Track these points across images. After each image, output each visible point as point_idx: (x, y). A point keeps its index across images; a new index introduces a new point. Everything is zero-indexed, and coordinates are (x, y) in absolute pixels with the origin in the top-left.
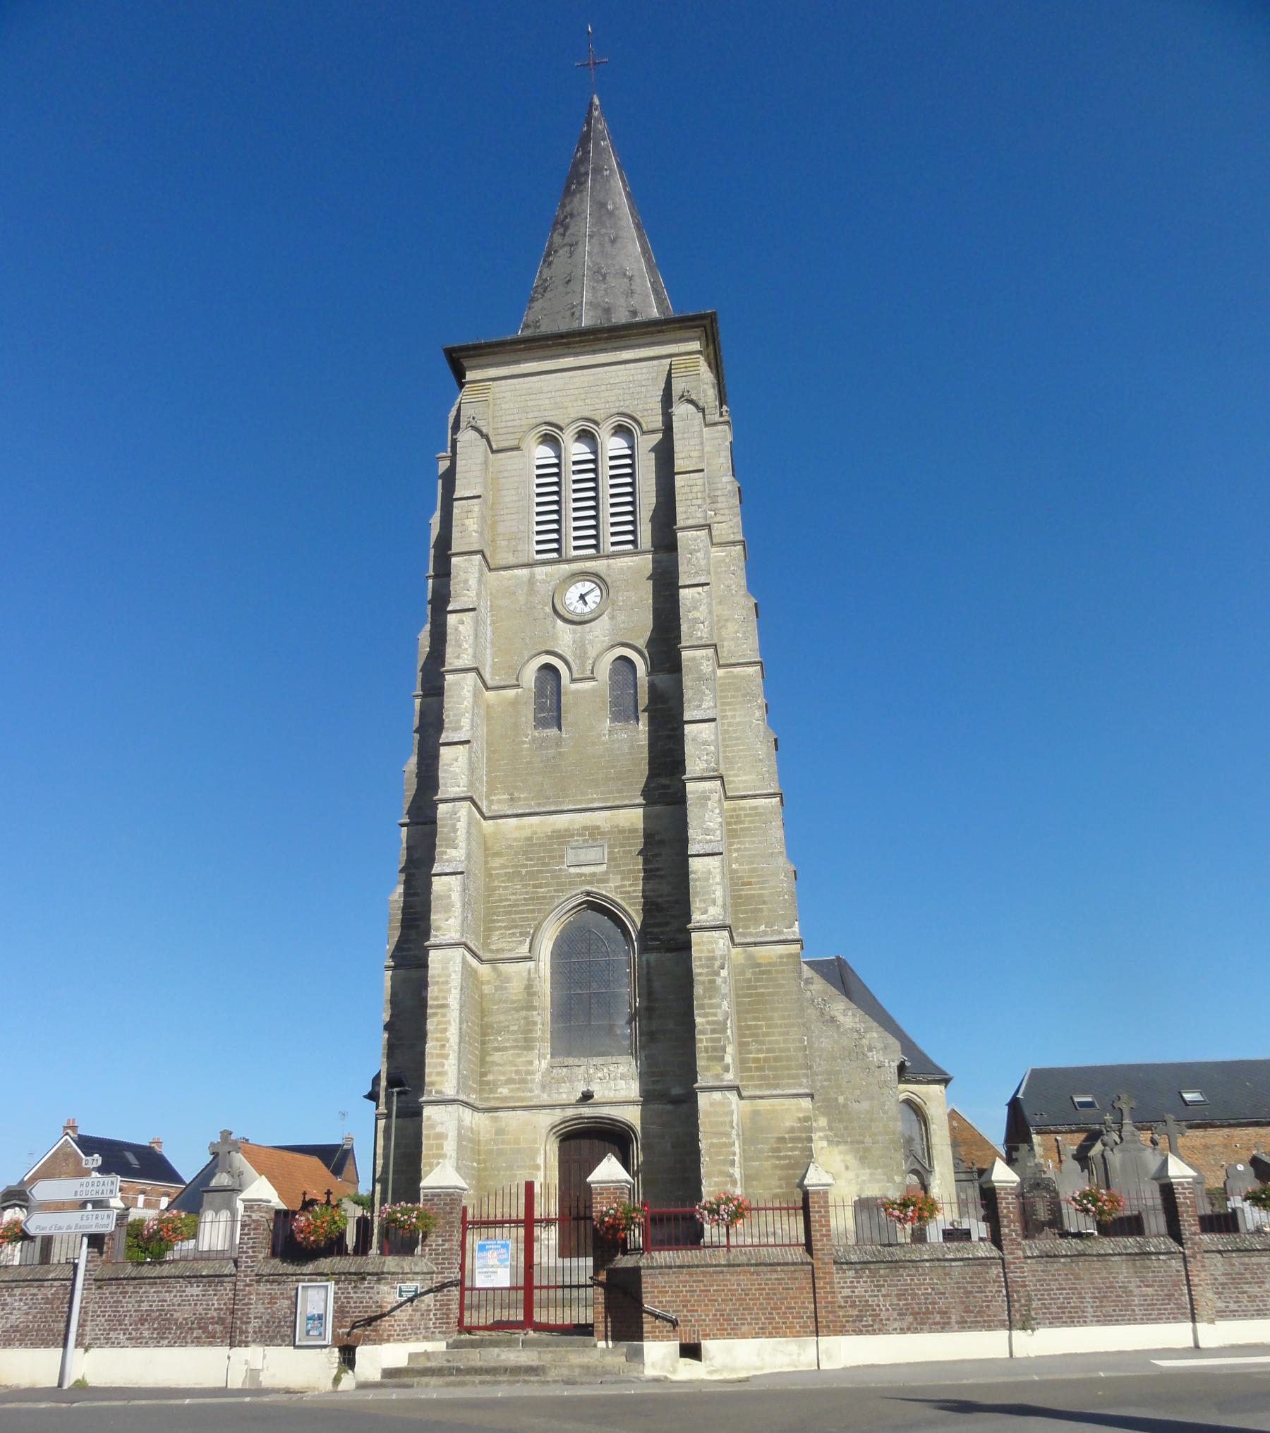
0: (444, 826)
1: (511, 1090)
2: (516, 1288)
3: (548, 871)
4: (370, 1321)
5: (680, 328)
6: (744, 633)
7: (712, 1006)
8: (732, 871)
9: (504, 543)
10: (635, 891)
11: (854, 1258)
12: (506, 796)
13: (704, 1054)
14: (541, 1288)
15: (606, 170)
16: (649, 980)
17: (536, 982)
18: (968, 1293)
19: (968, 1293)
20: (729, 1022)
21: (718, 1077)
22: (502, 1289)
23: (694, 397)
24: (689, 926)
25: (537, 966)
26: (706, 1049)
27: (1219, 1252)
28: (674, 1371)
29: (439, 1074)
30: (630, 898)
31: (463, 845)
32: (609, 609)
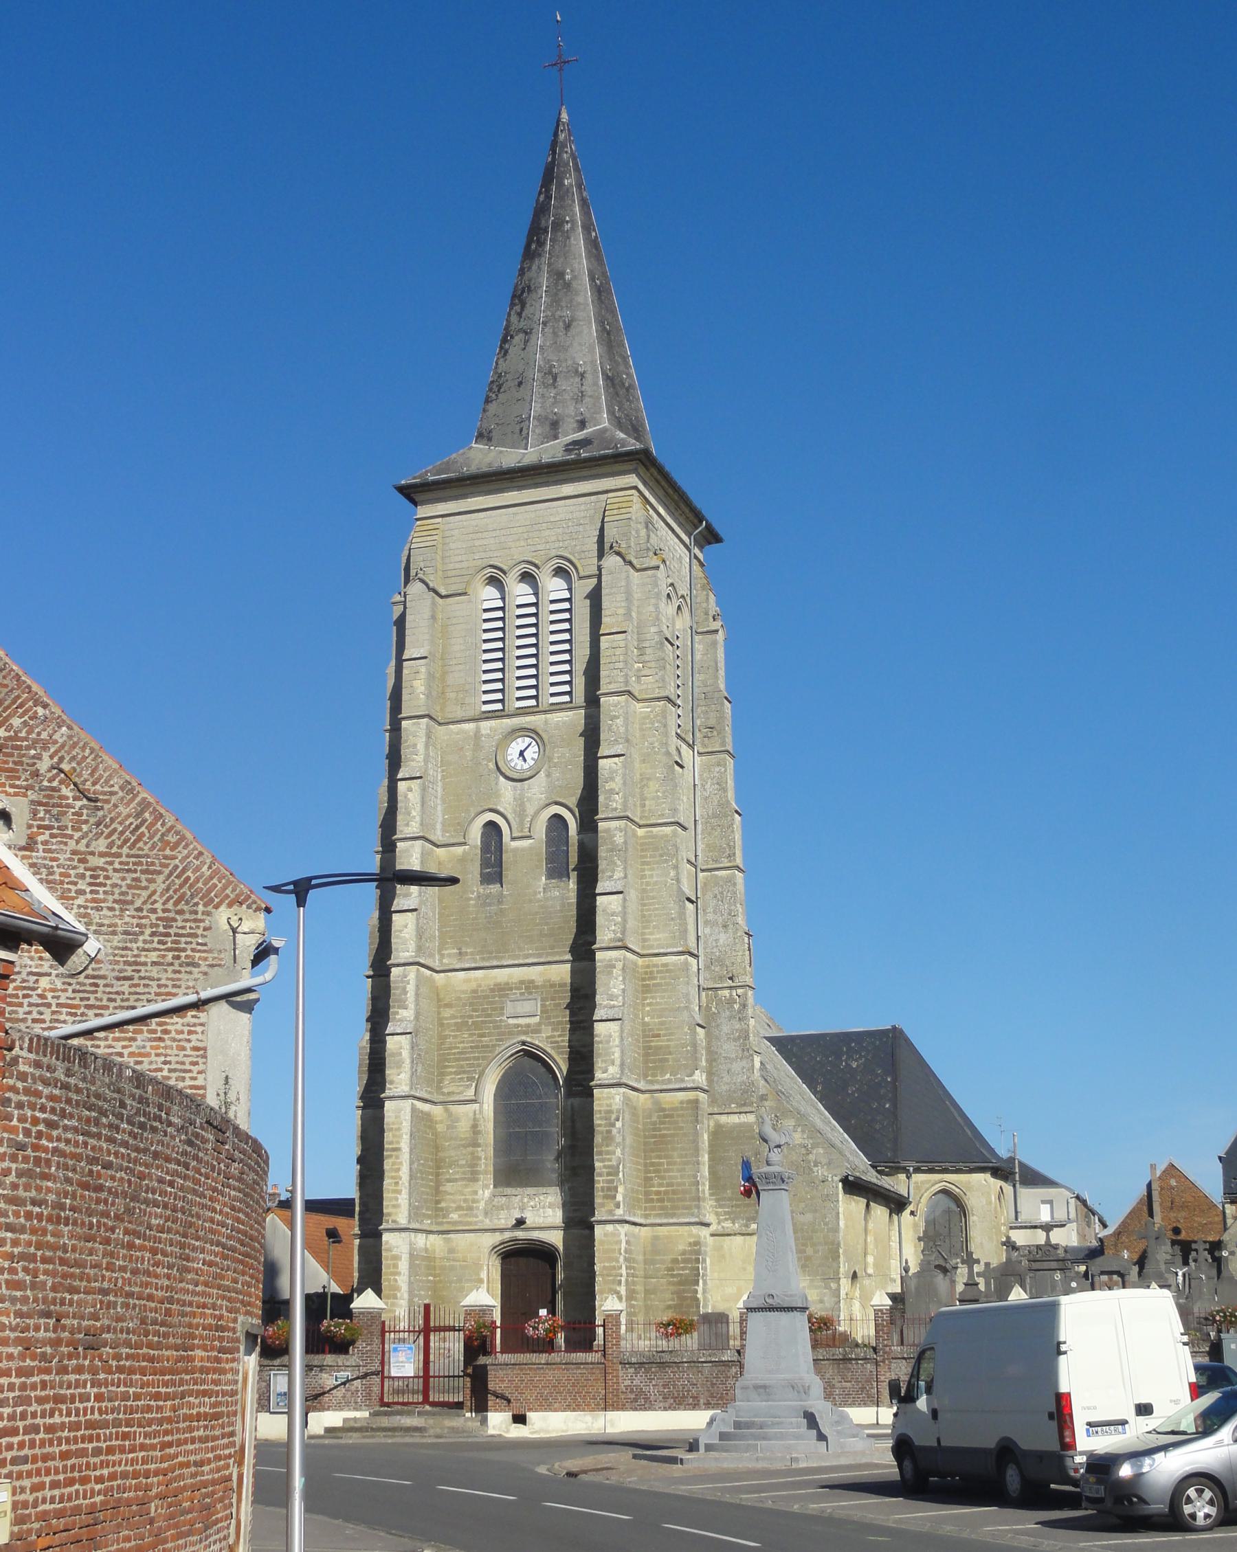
0: (397, 988)
1: (460, 1216)
2: (418, 1377)
3: (490, 1022)
4: (316, 1397)
5: (616, 462)
6: (664, 792)
7: (608, 1153)
8: (644, 1024)
9: (453, 695)
10: (563, 1041)
11: (634, 1360)
12: (455, 951)
13: (600, 1193)
14: (434, 1377)
15: (567, 222)
16: (573, 1121)
17: (481, 1121)
18: (713, 1385)
19: (713, 1385)
20: (621, 1167)
21: (611, 1212)
22: (409, 1377)
23: (623, 551)
24: (592, 1083)
25: (481, 1107)
26: (603, 1190)
27: (904, 1358)
28: (508, 1431)
29: (394, 1206)
30: (559, 1047)
31: (412, 1006)
32: (546, 766)
